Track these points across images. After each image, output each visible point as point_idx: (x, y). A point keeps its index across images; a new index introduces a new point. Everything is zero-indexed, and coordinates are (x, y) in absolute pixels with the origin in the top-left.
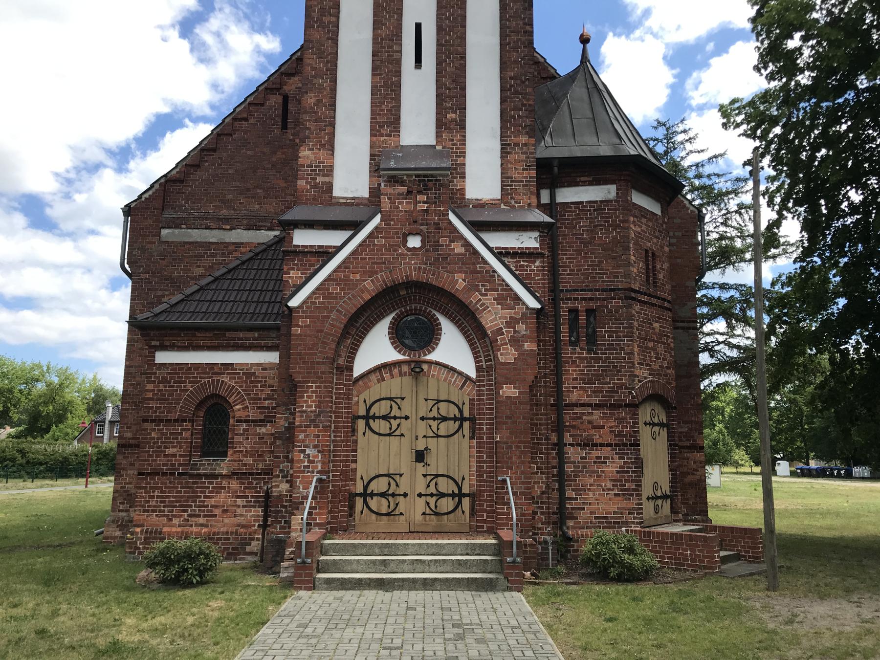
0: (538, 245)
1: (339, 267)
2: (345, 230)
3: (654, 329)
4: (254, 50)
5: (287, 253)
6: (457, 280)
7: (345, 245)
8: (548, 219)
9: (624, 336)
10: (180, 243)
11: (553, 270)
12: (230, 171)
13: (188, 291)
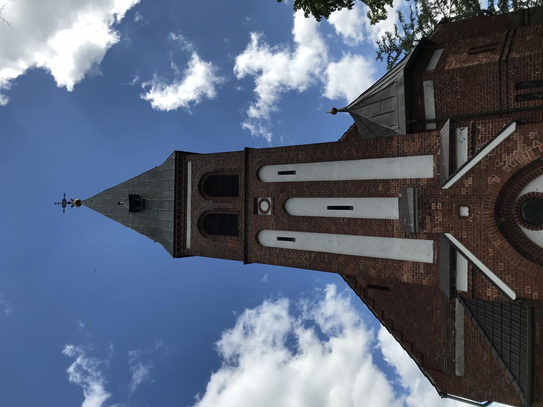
0: (466, 128)
1: (484, 263)
2: (456, 257)
3: (531, 39)
4: (335, 300)
5: (473, 296)
6: (493, 182)
7: (467, 258)
8: (448, 123)
9: (538, 60)
10: (465, 364)
11: (483, 116)
12: (415, 325)
13: (503, 365)
